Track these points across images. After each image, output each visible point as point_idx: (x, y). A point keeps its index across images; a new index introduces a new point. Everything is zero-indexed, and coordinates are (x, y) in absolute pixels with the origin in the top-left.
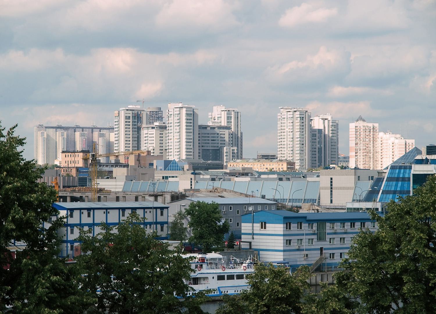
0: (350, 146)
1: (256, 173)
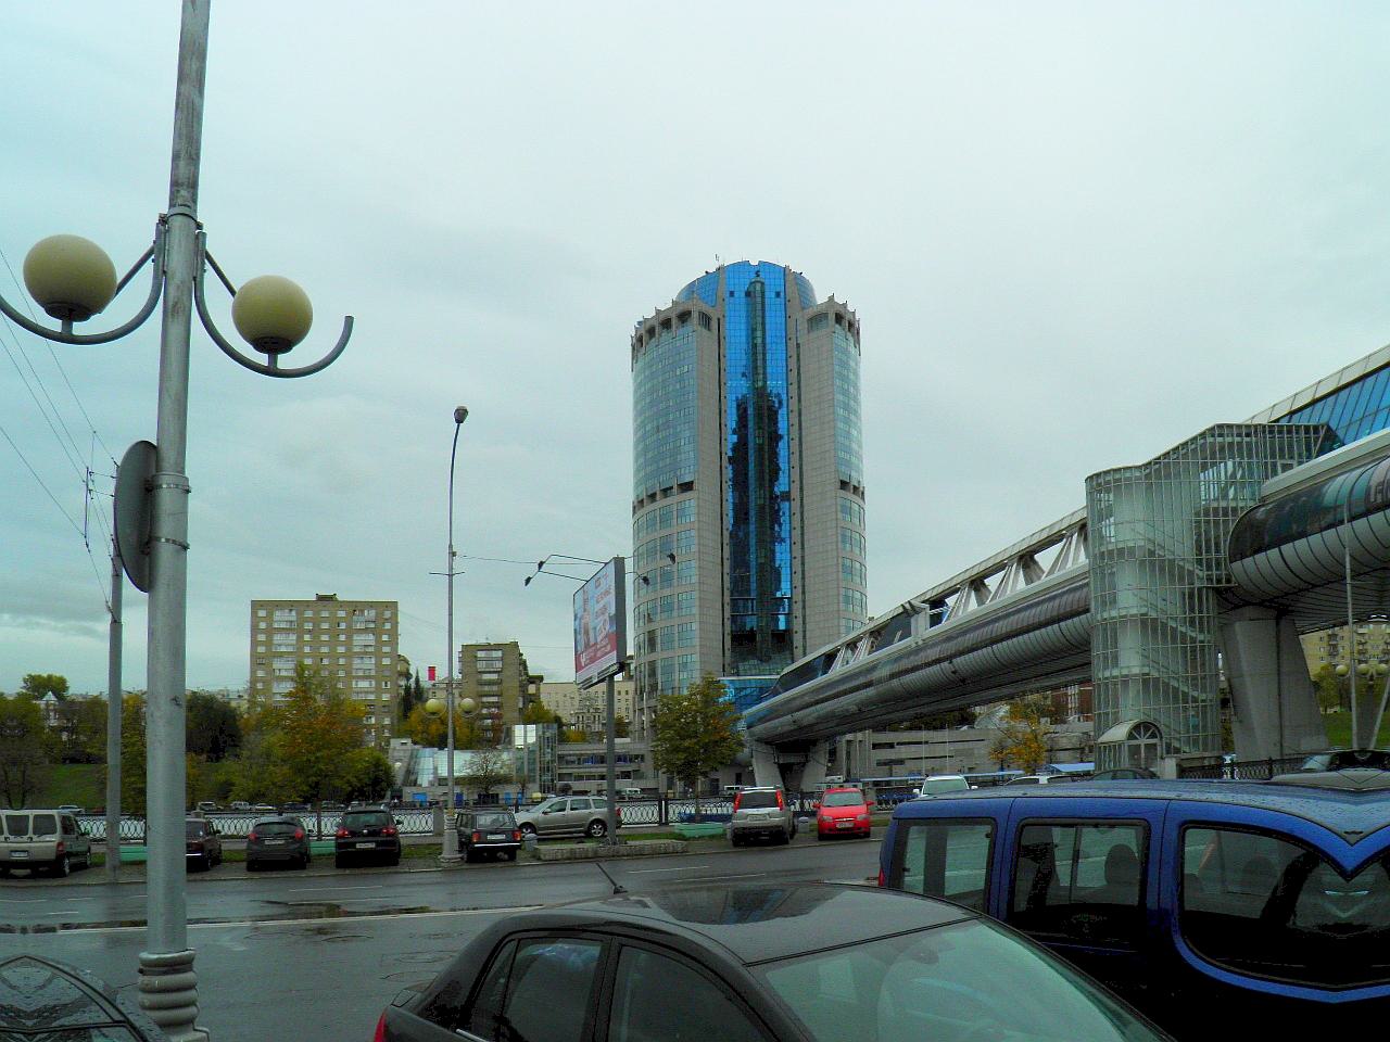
0: (1186, 872)
1: (1003, 906)
